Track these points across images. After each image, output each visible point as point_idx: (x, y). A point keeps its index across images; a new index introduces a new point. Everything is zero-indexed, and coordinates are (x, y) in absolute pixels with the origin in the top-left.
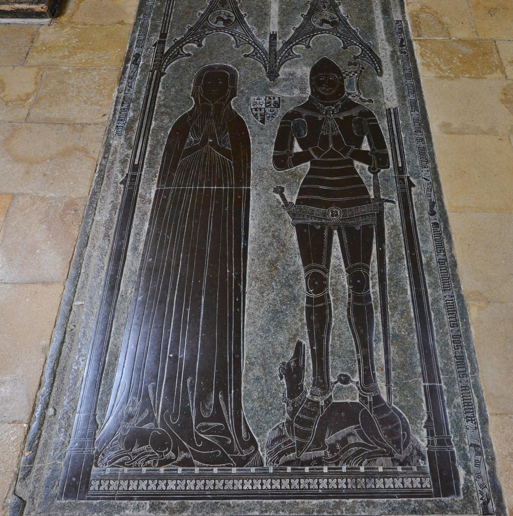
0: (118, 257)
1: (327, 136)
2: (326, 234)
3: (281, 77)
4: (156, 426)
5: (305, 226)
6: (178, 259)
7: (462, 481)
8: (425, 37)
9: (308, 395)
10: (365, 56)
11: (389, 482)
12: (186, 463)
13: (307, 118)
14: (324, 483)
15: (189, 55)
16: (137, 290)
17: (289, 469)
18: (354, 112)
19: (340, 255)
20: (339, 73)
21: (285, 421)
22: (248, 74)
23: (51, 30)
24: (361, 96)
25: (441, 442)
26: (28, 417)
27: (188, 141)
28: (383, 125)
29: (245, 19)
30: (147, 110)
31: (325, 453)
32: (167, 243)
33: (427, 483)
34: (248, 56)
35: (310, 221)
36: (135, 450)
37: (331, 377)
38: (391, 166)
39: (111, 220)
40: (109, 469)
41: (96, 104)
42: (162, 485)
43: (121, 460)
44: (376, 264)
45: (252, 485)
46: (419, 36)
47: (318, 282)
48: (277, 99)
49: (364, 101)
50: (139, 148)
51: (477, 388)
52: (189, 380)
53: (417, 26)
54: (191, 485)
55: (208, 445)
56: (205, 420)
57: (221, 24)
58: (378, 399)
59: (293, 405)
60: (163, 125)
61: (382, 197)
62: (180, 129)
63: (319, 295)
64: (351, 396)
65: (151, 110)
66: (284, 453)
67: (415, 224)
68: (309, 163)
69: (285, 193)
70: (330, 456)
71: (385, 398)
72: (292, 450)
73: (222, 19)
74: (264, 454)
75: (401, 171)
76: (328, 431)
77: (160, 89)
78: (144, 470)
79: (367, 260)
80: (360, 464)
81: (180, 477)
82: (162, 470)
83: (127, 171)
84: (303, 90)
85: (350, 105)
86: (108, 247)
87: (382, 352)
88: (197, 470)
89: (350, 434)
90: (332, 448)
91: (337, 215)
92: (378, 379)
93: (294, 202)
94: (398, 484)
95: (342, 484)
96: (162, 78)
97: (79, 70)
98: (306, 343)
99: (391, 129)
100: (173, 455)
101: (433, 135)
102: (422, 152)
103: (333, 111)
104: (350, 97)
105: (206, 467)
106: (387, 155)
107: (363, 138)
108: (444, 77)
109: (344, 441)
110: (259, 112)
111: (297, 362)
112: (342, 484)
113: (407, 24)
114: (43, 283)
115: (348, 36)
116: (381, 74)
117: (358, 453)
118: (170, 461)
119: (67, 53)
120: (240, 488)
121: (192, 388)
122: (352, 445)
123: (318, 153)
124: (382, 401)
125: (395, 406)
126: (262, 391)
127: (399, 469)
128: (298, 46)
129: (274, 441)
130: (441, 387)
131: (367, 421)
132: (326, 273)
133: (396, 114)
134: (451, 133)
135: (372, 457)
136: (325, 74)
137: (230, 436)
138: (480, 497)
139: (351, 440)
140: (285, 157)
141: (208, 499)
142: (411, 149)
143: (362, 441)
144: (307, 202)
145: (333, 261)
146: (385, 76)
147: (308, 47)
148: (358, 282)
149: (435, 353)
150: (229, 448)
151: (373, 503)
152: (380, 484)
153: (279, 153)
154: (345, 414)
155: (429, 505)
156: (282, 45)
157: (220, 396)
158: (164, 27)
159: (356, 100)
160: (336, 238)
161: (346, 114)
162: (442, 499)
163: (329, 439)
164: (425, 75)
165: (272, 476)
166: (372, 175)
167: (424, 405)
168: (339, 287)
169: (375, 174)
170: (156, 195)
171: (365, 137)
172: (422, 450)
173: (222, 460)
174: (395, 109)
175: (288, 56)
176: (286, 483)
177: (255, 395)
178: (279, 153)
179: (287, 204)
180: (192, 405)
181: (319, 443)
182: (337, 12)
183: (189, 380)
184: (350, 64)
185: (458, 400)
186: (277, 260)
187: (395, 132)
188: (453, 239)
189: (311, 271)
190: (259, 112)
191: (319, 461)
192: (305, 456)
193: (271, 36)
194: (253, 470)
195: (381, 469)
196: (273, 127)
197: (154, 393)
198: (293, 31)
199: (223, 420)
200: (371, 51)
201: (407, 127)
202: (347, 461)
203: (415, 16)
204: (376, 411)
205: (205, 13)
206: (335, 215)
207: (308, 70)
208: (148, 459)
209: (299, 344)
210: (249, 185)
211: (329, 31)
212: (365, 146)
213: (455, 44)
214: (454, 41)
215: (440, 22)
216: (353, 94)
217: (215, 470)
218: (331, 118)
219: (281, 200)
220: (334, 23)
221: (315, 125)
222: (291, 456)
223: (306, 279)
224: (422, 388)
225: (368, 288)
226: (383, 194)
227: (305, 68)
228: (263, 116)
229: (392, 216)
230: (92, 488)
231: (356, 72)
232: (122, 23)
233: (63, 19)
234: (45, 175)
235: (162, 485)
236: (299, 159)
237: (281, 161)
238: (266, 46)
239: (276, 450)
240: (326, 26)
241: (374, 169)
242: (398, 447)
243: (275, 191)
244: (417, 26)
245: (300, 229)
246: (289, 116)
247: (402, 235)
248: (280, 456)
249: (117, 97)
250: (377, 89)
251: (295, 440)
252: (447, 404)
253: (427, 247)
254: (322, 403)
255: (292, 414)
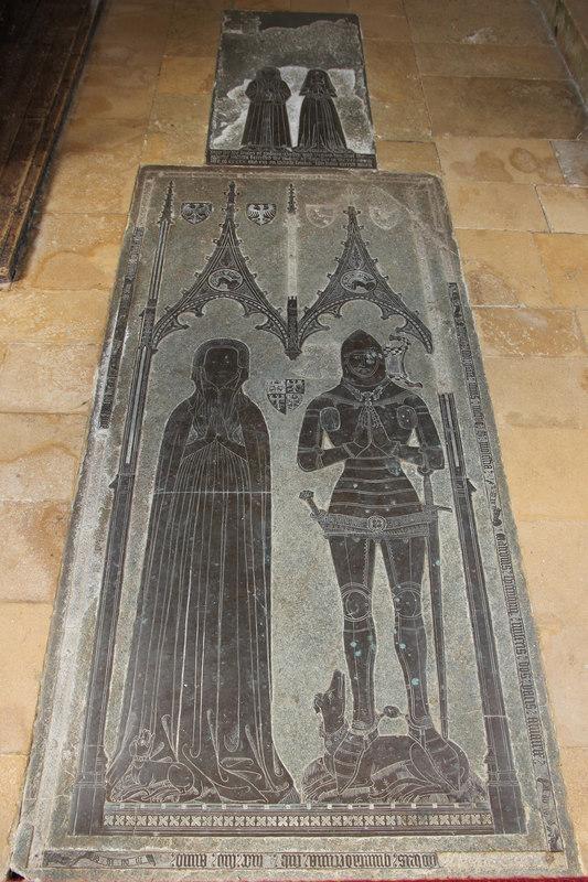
0: (113, 577)
1: (366, 431)
2: (367, 548)
3: (304, 354)
4: (175, 760)
5: (340, 539)
6: (187, 578)
7: (528, 818)
8: (487, 305)
9: (350, 729)
10: (272, 325)
11: (444, 819)
12: (212, 799)
13: (338, 406)
14: (370, 821)
15: (186, 327)
16: (139, 612)
17: (330, 806)
18: (398, 399)
19: (385, 572)
20: (378, 349)
21: (323, 756)
22: (263, 348)
23: (11, 297)
24: (408, 379)
25: (503, 778)
26: (27, 747)
27: (190, 435)
28: (436, 414)
29: (256, 280)
30: (137, 397)
31: (371, 789)
32: (172, 558)
33: (489, 820)
34: (261, 328)
35: (346, 533)
36: (152, 784)
37: (376, 710)
38: (447, 466)
39: (102, 530)
40: (123, 804)
41: (74, 389)
42: (185, 821)
43: (136, 795)
44: (428, 583)
45: (288, 822)
46: (479, 302)
47: (357, 604)
48: (300, 383)
49: (412, 385)
50: (131, 444)
51: (546, 718)
52: (209, 712)
53: (476, 291)
54: (218, 821)
55: (235, 780)
56: (230, 755)
57: (224, 288)
58: (431, 732)
59: (332, 740)
60: (159, 411)
61: (435, 504)
62: (181, 421)
63: (362, 619)
64: (400, 728)
65: (142, 396)
66: (324, 789)
67: (476, 536)
68: (342, 464)
69: (315, 500)
70: (376, 793)
71: (438, 729)
72: (334, 787)
73: (227, 282)
74: (299, 789)
75: (458, 471)
76: (374, 765)
77: (152, 370)
78: (164, 806)
79: (418, 579)
80: (412, 801)
81: (205, 813)
82: (184, 806)
83: (116, 471)
84: (332, 370)
85: (394, 390)
86: (100, 560)
87: (436, 682)
88: (224, 807)
89: (400, 770)
90: (379, 785)
91: (379, 526)
92: (431, 712)
93: (326, 508)
94: (455, 820)
95: (391, 821)
96: (154, 356)
97: (49, 347)
98: (345, 671)
99: (446, 421)
100: (196, 790)
101: (498, 427)
102: (484, 447)
103: (372, 397)
104: (393, 380)
105: (235, 804)
106: (441, 452)
107: (410, 431)
108: (511, 356)
109: (392, 777)
110: (278, 399)
111: (335, 693)
112: (391, 821)
113: (463, 287)
114: (28, 602)
115: (390, 303)
116: (431, 351)
117: (409, 789)
118: (192, 797)
119: (33, 326)
120: (275, 824)
121: (213, 720)
122: (401, 782)
123: (355, 450)
124: (437, 735)
125: (452, 740)
126: (295, 724)
127: (456, 805)
128: (325, 315)
129: (310, 777)
130: (505, 720)
131: (419, 756)
132: (368, 593)
133: (451, 401)
134: (521, 426)
135: (425, 793)
136: (357, 346)
137: (260, 771)
138: (548, 833)
139: (402, 776)
140: (313, 456)
141: (239, 835)
142: (470, 445)
143: (413, 777)
144: (343, 511)
145: (376, 579)
146: (437, 354)
147: (338, 316)
148: (407, 608)
149: (499, 683)
150: (259, 783)
151: (427, 840)
152: (434, 821)
153: (306, 450)
154: (396, 747)
155: (490, 842)
156: (303, 314)
157: (247, 730)
158: (153, 292)
159: (401, 384)
160: (379, 552)
161: (389, 402)
162: (505, 835)
163: (375, 775)
164: (488, 353)
165: (311, 813)
166: (422, 478)
167: (485, 738)
168: (384, 610)
169: (426, 476)
170: (154, 501)
171: (414, 430)
172: (482, 786)
173: (254, 797)
174: (451, 396)
175: (315, 327)
176: (326, 820)
177: (288, 729)
178: (306, 450)
179: (317, 513)
180: (214, 738)
181: (363, 779)
182: (374, 271)
183: (209, 712)
184: (392, 338)
185: (525, 733)
186: (307, 578)
187: (451, 422)
188: (522, 553)
189: (350, 592)
190: (278, 399)
191: (365, 798)
192: (347, 792)
193: (290, 302)
194: (288, 807)
195: (435, 806)
196: (298, 415)
197: (169, 725)
198: (318, 296)
199: (251, 755)
200: (419, 322)
201: (465, 419)
202: (396, 798)
203: (475, 279)
204: (429, 745)
205: (204, 273)
206: (377, 526)
207: (338, 346)
208: (168, 794)
209: (337, 674)
210: (269, 489)
211: (363, 296)
212: (413, 442)
213: (525, 314)
214: (523, 309)
215: (505, 286)
216: (397, 376)
217: (245, 807)
218: (369, 403)
219: (309, 508)
220: (369, 286)
221: (348, 416)
222: (332, 792)
223: (344, 600)
224: (484, 722)
225: (419, 610)
226: (438, 500)
227: (334, 343)
228: (283, 403)
229: (448, 527)
230: (105, 823)
231: (400, 349)
232: (99, 286)
233: (26, 282)
234: (18, 476)
235: (185, 821)
236: (330, 458)
237: (308, 462)
238: (284, 314)
239: (316, 785)
240: (360, 290)
241: (425, 469)
242: (455, 782)
243: (302, 496)
244: (476, 291)
245: (334, 541)
246: (316, 405)
247: (460, 549)
248: (319, 792)
249: (99, 381)
250: (427, 369)
251: (335, 776)
252: (421, 550)
253: (490, 559)
254: (366, 738)
255: (331, 750)
